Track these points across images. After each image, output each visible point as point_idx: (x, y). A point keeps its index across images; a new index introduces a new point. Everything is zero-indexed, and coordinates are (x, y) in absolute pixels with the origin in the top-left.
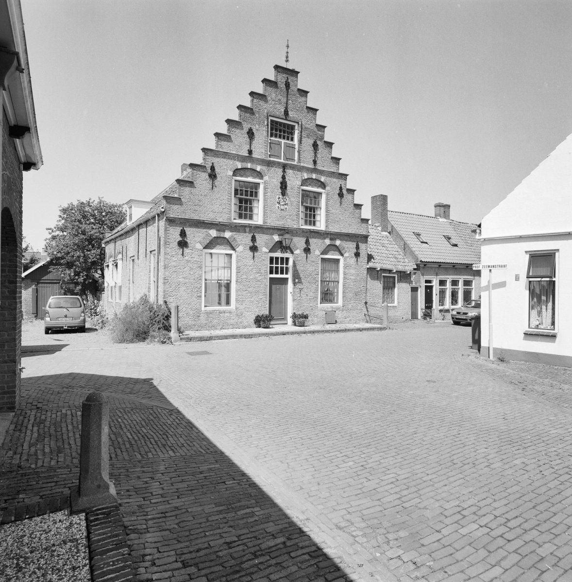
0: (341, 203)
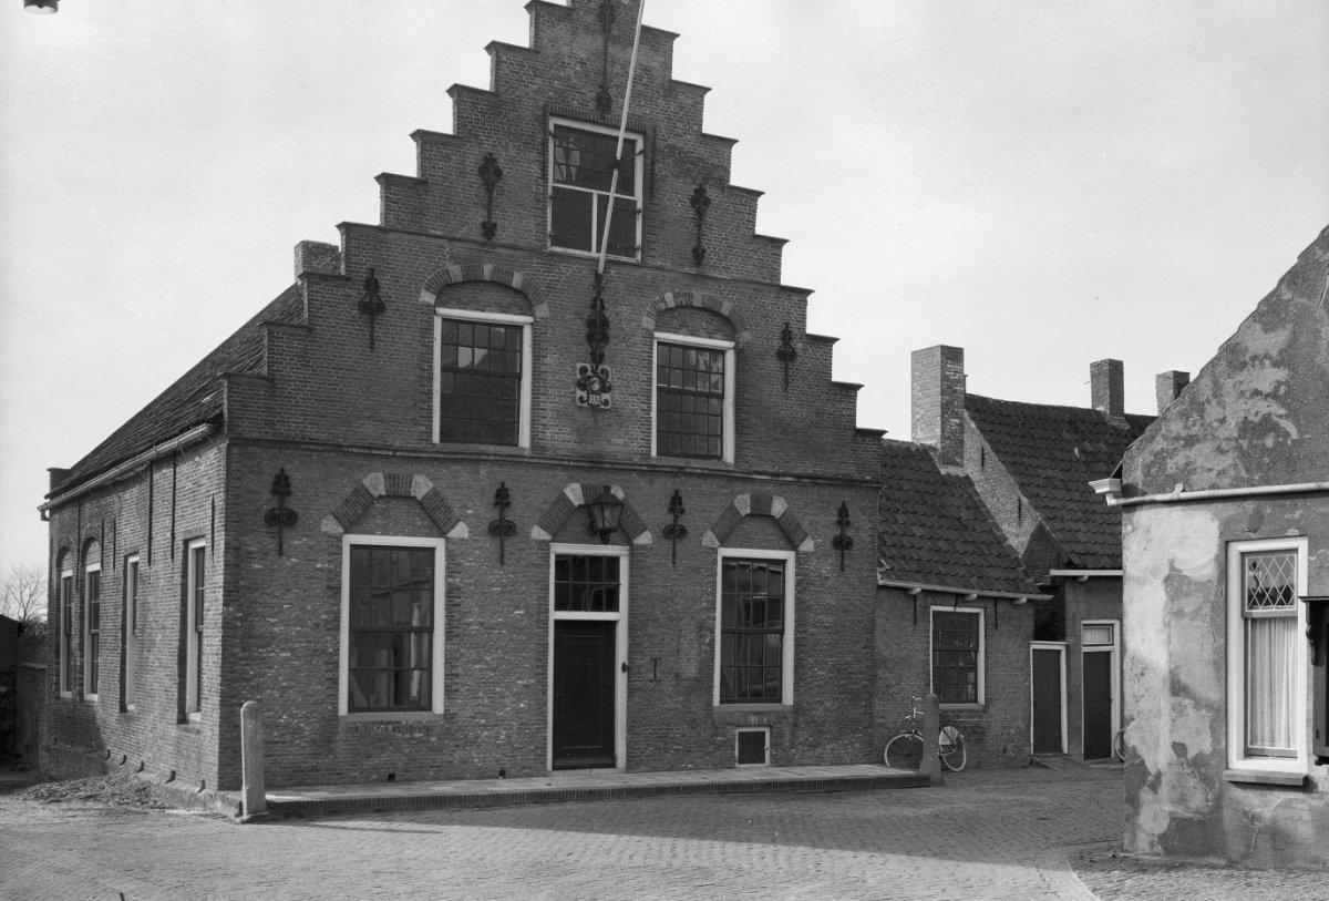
0: (786, 382)
